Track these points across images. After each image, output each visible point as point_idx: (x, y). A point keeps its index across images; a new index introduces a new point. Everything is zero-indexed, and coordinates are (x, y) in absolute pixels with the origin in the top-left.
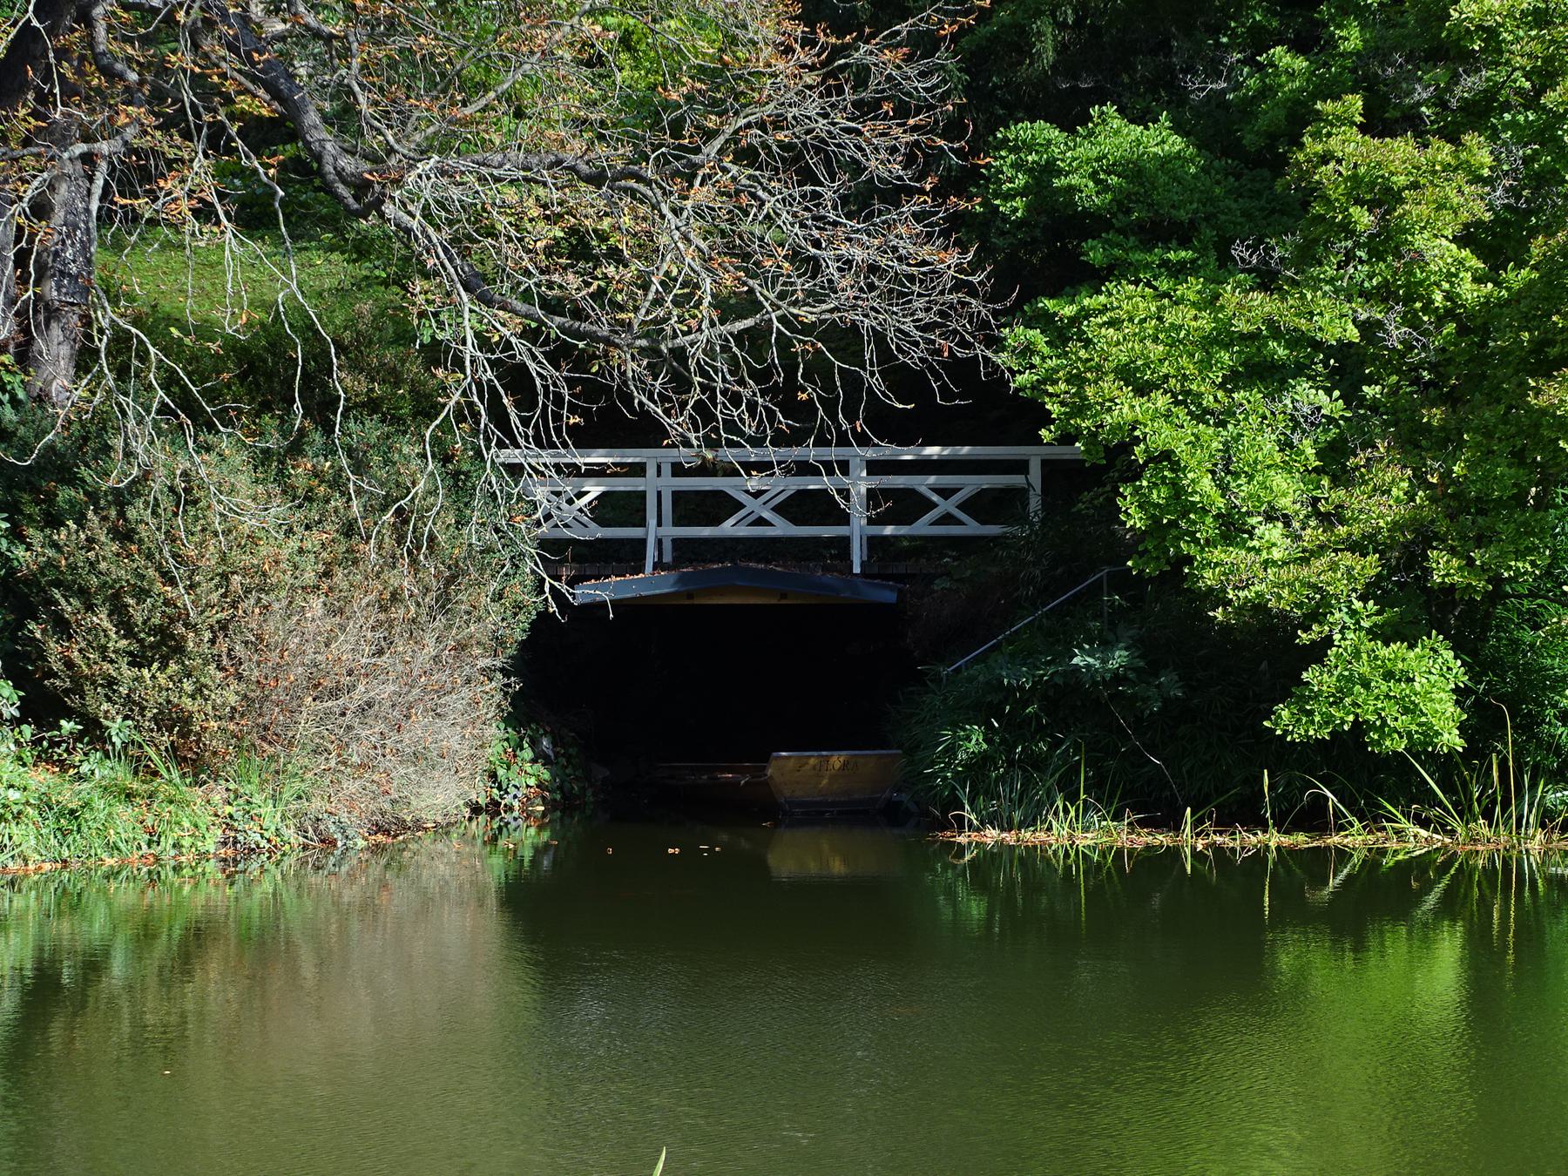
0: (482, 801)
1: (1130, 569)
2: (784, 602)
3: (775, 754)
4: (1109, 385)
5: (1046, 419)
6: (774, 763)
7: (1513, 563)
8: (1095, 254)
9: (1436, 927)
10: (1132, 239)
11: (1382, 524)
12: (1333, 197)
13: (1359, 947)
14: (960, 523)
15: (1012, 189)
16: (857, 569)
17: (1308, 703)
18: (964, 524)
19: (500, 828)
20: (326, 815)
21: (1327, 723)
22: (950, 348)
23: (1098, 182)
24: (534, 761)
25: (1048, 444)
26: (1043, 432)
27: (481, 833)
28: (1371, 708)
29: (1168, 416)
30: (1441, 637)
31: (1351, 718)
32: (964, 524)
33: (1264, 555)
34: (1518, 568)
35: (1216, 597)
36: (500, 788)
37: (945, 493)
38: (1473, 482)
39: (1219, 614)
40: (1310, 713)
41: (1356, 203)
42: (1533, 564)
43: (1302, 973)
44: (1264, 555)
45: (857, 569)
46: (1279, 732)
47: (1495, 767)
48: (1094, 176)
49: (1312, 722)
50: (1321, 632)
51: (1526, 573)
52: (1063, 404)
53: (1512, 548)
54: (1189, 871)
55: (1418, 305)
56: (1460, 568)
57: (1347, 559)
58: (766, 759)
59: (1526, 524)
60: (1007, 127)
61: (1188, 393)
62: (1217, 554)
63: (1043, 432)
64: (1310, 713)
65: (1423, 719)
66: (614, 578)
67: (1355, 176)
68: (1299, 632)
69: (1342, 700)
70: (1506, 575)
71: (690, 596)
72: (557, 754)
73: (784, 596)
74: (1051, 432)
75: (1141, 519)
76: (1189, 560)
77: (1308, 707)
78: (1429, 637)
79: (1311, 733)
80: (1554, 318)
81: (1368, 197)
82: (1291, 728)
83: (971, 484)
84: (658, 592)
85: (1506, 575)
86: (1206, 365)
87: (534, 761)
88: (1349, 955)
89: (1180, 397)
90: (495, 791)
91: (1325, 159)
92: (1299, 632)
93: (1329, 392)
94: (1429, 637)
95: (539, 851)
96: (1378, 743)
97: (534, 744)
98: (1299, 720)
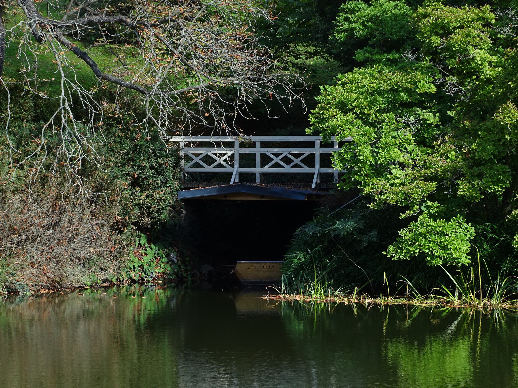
0: (136, 278)
1: (338, 187)
2: (262, 199)
3: (238, 262)
4: (332, 111)
5: (308, 125)
6: (238, 265)
7: (492, 187)
8: (359, 55)
9: (456, 340)
10: (376, 49)
11: (439, 169)
12: (424, 32)
13: (421, 346)
14: (225, 167)
15: (341, 29)
16: (313, 186)
17: (400, 244)
18: (225, 167)
19: (145, 290)
20: (15, 282)
21: (408, 253)
22: (274, 95)
23: (364, 25)
24: (167, 263)
25: (308, 135)
26: (307, 130)
27: (137, 291)
28: (427, 247)
29: (352, 123)
30: (462, 217)
31: (418, 250)
32: (225, 167)
33: (393, 181)
34: (495, 189)
35: (369, 198)
36: (145, 273)
37: (277, 155)
38: (478, 152)
39: (371, 205)
40: (401, 249)
41: (434, 35)
42: (502, 187)
43: (396, 358)
44: (393, 181)
45: (313, 186)
46: (389, 256)
47: (472, 272)
48: (363, 24)
49: (402, 252)
50: (410, 214)
51: (498, 191)
52: (316, 118)
53: (490, 180)
54: (356, 313)
55: (474, 77)
56: (469, 189)
57: (422, 183)
58: (235, 263)
59: (497, 170)
60: (345, 3)
61: (364, 114)
62: (369, 180)
63: (307, 130)
64: (401, 249)
65: (449, 252)
66: (195, 189)
67: (436, 23)
68: (401, 214)
69: (414, 243)
70: (490, 191)
71: (226, 196)
72: (178, 260)
73: (262, 197)
74: (310, 129)
75: (341, 166)
76: (360, 183)
77: (400, 246)
78: (456, 217)
79: (401, 257)
80: (510, 83)
81: (441, 32)
82: (394, 255)
83: (286, 151)
84: (210, 194)
85: (490, 191)
86: (372, 103)
87: (167, 263)
88: (416, 350)
89: (360, 116)
90: (143, 274)
91: (425, 16)
92: (401, 214)
93: (434, 114)
94: (456, 217)
95: (169, 299)
96: (430, 262)
97: (168, 255)
98: (397, 251)
